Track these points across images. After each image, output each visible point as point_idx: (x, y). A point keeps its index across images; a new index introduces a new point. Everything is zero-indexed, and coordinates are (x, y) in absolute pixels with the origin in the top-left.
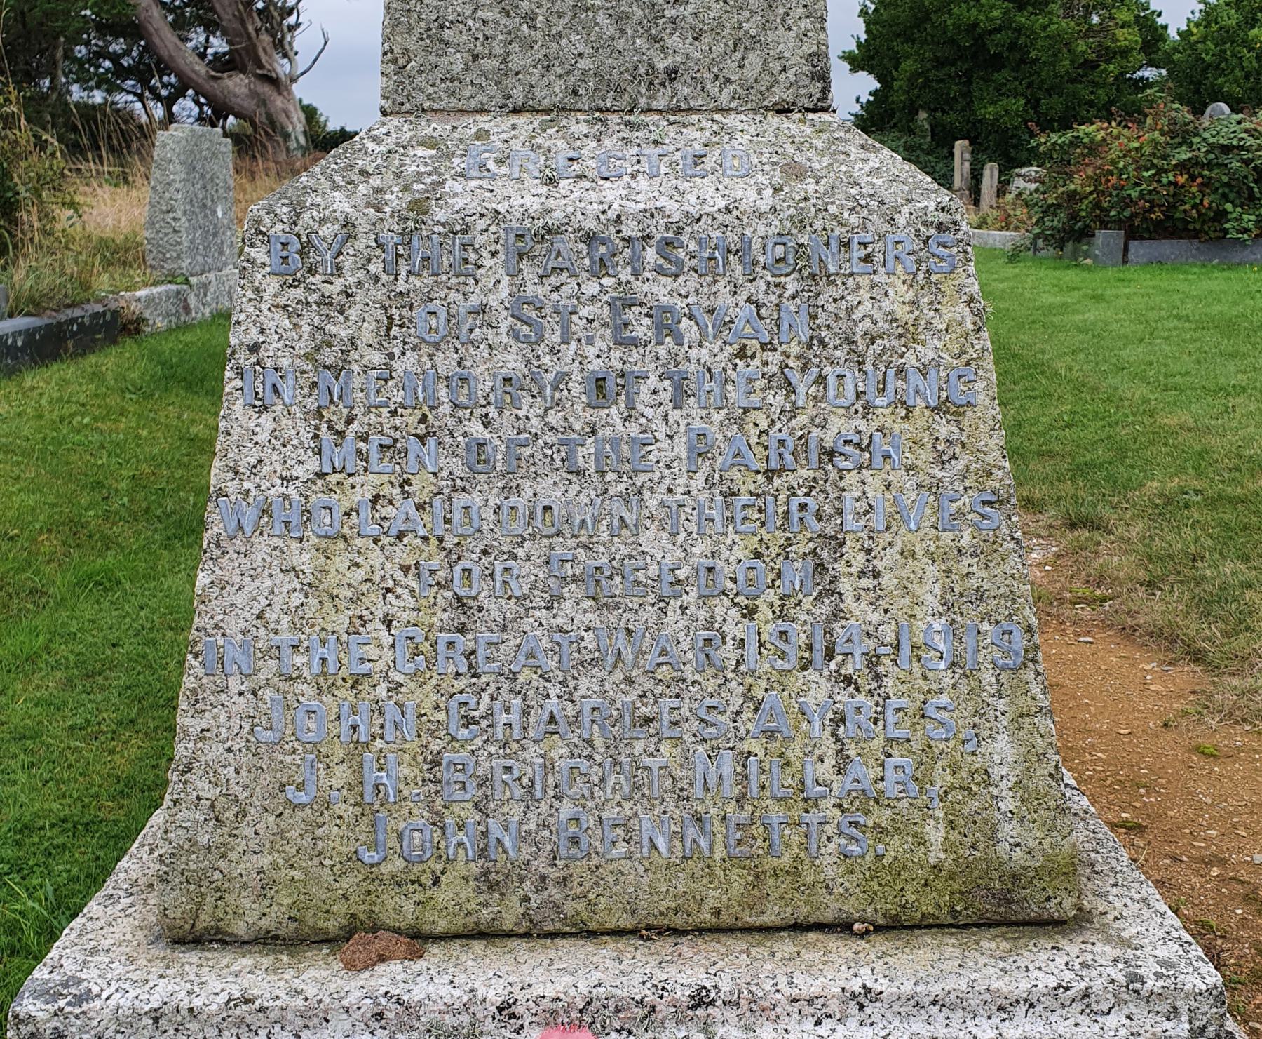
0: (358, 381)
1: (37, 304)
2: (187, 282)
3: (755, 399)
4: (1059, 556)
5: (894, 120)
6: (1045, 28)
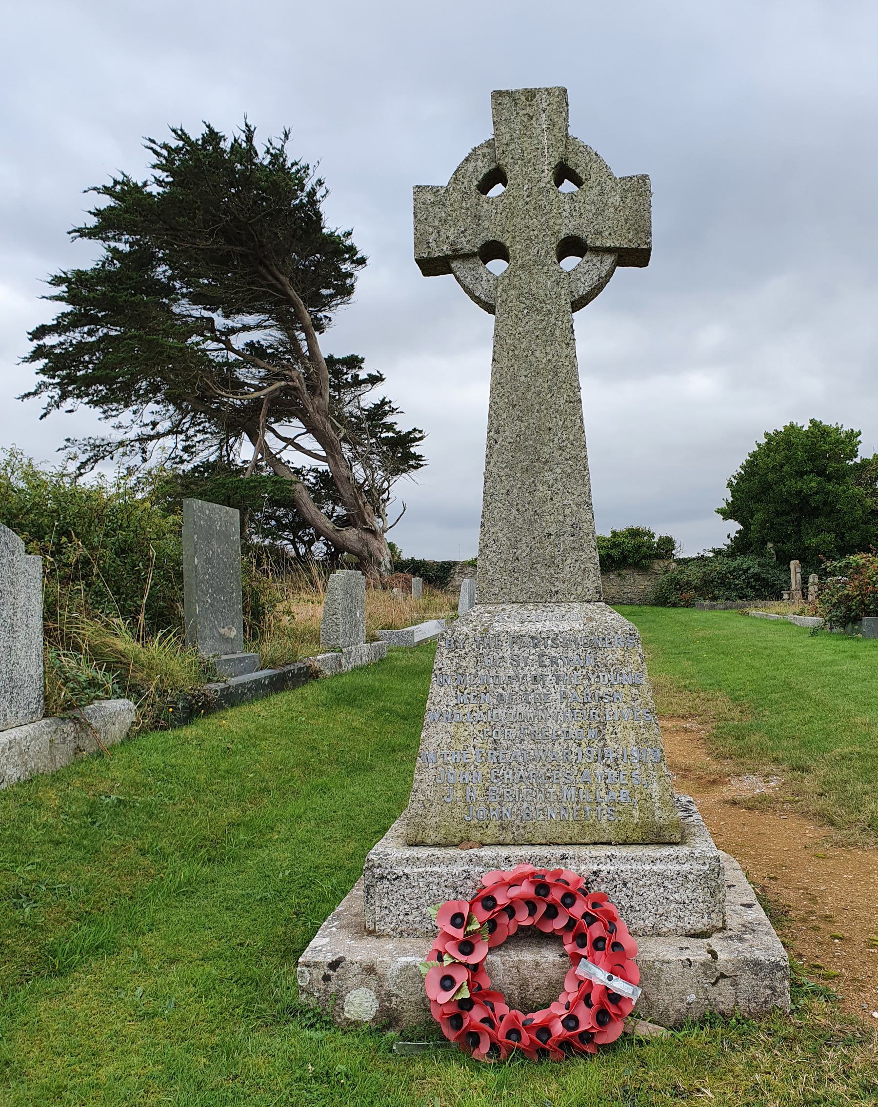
0: (468, 678)
1: (274, 664)
2: (341, 651)
3: (580, 682)
4: (784, 784)
5: (752, 548)
6: (844, 492)
